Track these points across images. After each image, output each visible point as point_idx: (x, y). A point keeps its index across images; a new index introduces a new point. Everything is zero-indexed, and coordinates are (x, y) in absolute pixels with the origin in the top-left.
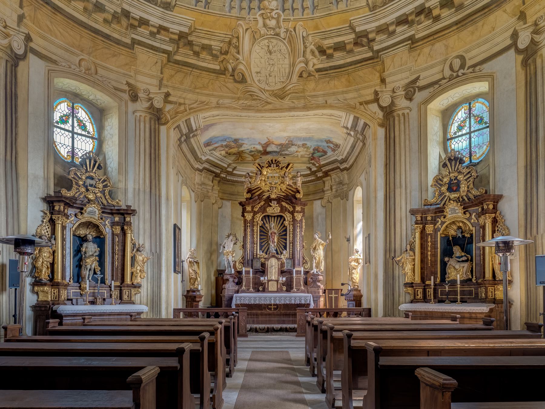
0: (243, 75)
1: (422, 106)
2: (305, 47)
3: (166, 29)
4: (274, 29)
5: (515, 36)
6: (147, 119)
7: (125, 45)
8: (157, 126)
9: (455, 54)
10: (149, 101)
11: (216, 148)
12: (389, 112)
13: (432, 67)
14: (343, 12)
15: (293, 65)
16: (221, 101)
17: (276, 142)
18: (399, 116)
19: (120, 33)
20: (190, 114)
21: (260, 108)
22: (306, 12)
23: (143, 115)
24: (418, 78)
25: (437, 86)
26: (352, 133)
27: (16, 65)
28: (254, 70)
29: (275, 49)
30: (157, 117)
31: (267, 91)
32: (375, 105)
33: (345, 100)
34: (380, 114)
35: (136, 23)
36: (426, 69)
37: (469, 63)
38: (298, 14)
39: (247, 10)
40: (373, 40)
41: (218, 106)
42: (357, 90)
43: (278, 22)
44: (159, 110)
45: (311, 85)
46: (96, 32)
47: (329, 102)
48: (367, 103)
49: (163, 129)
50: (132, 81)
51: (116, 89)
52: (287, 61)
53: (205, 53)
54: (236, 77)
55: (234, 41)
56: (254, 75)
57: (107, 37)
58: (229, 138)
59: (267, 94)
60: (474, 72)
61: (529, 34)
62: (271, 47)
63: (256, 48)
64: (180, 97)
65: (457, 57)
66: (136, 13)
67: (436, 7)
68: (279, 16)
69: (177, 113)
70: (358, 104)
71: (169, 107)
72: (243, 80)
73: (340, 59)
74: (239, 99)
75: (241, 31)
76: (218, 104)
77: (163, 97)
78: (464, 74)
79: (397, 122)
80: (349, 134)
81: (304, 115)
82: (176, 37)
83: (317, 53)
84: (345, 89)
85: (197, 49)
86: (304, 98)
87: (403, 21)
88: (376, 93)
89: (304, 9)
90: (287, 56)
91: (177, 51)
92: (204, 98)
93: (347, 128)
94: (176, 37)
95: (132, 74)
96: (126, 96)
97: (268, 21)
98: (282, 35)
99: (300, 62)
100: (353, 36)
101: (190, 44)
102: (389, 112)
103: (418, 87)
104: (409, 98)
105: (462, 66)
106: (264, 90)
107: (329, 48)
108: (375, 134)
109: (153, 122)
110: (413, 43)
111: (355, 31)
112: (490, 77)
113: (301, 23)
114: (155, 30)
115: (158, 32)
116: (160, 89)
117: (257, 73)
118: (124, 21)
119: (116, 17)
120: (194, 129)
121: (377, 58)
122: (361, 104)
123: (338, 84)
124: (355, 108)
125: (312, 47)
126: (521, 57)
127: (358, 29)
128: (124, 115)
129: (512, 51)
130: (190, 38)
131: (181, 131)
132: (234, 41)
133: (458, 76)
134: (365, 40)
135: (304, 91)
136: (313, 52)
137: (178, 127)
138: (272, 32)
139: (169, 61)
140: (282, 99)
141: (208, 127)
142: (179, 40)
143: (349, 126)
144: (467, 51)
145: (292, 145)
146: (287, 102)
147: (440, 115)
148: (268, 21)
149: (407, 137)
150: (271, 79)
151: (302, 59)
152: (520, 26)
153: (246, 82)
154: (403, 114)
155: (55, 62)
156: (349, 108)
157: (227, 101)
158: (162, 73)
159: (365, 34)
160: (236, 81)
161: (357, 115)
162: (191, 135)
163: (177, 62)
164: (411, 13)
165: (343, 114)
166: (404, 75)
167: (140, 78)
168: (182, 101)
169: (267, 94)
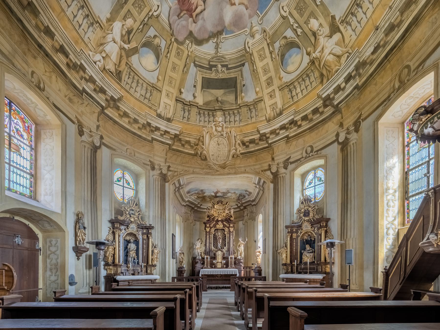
0: (205, 157)
2: (236, 142)
3: (168, 132)
4: (220, 132)
5: (337, 135)
6: (159, 179)
7: (148, 141)
9: (308, 145)
12: (276, 175)
13: (297, 151)
14: (254, 123)
15: (230, 151)
19: (145, 134)
20: (180, 177)
21: (213, 173)
22: (236, 123)
23: (158, 177)
26: (258, 186)
27: (96, 152)
28: (211, 154)
29: (221, 142)
30: (164, 178)
32: (269, 171)
34: (271, 176)
35: (154, 129)
36: (294, 153)
37: (315, 150)
38: (232, 124)
39: (233, 122)
40: (269, 138)
41: (193, 173)
42: (260, 164)
43: (222, 129)
45: (238, 161)
46: (134, 134)
48: (265, 170)
49: (167, 184)
50: (152, 160)
51: (144, 164)
52: (227, 149)
53: (187, 145)
55: (201, 138)
56: (211, 156)
57: (140, 136)
59: (217, 166)
60: (317, 154)
61: (344, 134)
62: (219, 142)
63: (212, 142)
64: (175, 168)
65: (309, 146)
66: (154, 124)
67: (299, 120)
68: (223, 125)
69: (174, 176)
70: (261, 171)
71: (170, 173)
72: (205, 159)
73: (252, 148)
74: (203, 169)
75: (205, 133)
78: (312, 155)
79: (279, 181)
80: (256, 187)
82: (173, 136)
83: (241, 145)
84: (254, 164)
85: (183, 142)
86: (235, 168)
87: (283, 127)
88: (270, 165)
89: (235, 122)
90: (227, 146)
91: (174, 144)
92: (187, 169)
93: (255, 184)
94: (173, 136)
95: (152, 156)
96: (149, 168)
97: (217, 128)
98: (225, 135)
99: (233, 149)
100: (259, 136)
101: (180, 140)
102: (276, 175)
104: (286, 168)
105: (312, 151)
107: (247, 142)
108: (269, 187)
109: (162, 181)
110: (288, 139)
111: (259, 133)
112: (325, 157)
113: (234, 129)
114: (163, 133)
115: (165, 134)
117: (212, 155)
118: (148, 129)
119: (143, 125)
121: (270, 147)
122: (262, 171)
123: (251, 161)
125: (239, 142)
126: (340, 146)
127: (261, 132)
129: (336, 144)
130: (180, 137)
131: (175, 186)
132: (201, 138)
133: (309, 156)
134: (264, 138)
135: (235, 164)
136: (239, 144)
137: (174, 183)
138: (220, 134)
139: (170, 149)
141: (188, 183)
142: (175, 138)
143: (256, 183)
144: (314, 143)
146: (226, 170)
148: (217, 128)
150: (219, 159)
151: (234, 148)
152: (340, 130)
154: (283, 176)
155: (114, 150)
156: (257, 173)
157: (197, 170)
159: (264, 135)
160: (202, 160)
163: (174, 150)
164: (287, 124)
166: (283, 156)
167: (156, 158)
168: (176, 170)
169: (217, 166)
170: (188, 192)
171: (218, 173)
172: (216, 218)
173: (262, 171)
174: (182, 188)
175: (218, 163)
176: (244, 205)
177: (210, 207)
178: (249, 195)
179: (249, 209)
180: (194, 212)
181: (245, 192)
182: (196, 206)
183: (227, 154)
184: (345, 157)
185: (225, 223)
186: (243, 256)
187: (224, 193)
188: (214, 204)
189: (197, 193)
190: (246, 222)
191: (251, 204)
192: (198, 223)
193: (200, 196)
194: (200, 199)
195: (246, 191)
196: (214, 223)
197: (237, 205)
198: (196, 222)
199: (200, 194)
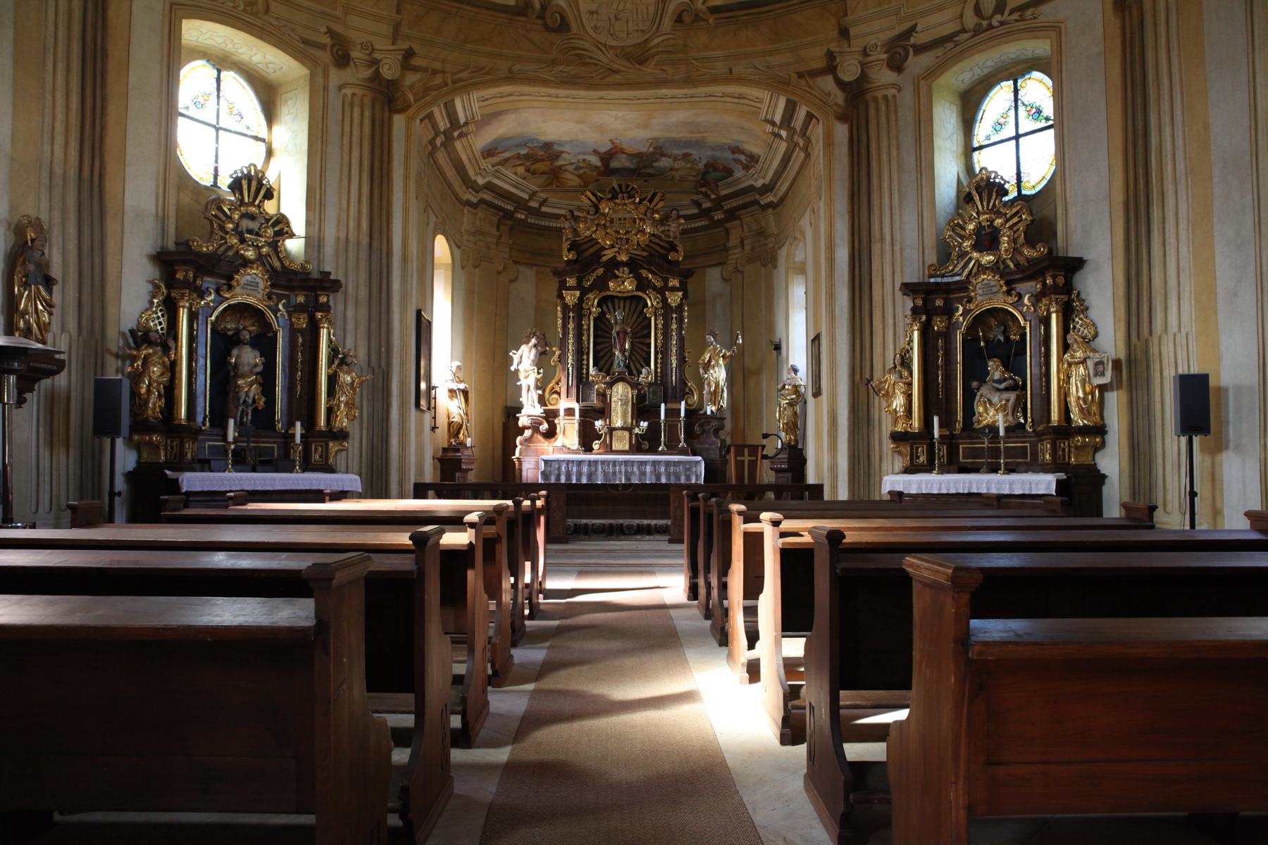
0: (562, 18)
1: (922, 83)
6: (367, 101)
8: (387, 114)
10: (370, 67)
11: (507, 160)
16: (517, 67)
17: (630, 150)
18: (876, 100)
20: (454, 91)
23: (360, 92)
24: (912, 29)
25: (950, 45)
26: (784, 133)
30: (386, 97)
31: (612, 47)
33: (768, 67)
34: (839, 97)
44: (392, 85)
47: (735, 70)
48: (814, 74)
49: (399, 121)
50: (339, 29)
51: (306, 42)
54: (549, 20)
56: (585, 17)
58: (532, 140)
59: (610, 54)
60: (1022, 19)
69: (427, 90)
70: (794, 76)
71: (411, 78)
74: (554, 63)
76: (510, 71)
77: (400, 57)
78: (1002, 23)
79: (872, 112)
80: (777, 135)
81: (686, 96)
88: (831, 56)
93: (773, 123)
95: (339, 13)
96: (325, 57)
103: (913, 46)
104: (897, 65)
106: (605, 45)
112: (1056, 29)
116: (393, 43)
117: (592, 13)
120: (462, 121)
122: (800, 75)
124: (788, 84)
128: (321, 93)
131: (434, 125)
133: (991, 27)
137: (430, 117)
140: (640, 64)
143: (778, 119)
145: (663, 155)
146: (650, 70)
147: (958, 102)
149: (894, 142)
153: (569, 30)
154: (885, 97)
156: (777, 84)
158: (398, 12)
160: (547, 28)
161: (794, 98)
162: (456, 134)
165: (765, 95)
168: (438, 66)
169: (610, 54)
170: (489, 153)
171: (617, 78)
172: (609, 254)
173: (800, 75)
174: (461, 135)
175: (614, 43)
176: (727, 205)
177: (579, 208)
178: (746, 168)
179: (747, 220)
180: (511, 229)
181: (728, 155)
182: (520, 204)
183: (652, 9)
184: (1132, 33)
185: (644, 273)
186: (724, 404)
187: (639, 155)
188: (600, 200)
189: (527, 157)
190: (737, 270)
191: (758, 203)
192: (528, 274)
193: (541, 167)
194: (541, 180)
195: (736, 150)
196: (601, 271)
197: (698, 205)
198: (522, 269)
199: (537, 161)
